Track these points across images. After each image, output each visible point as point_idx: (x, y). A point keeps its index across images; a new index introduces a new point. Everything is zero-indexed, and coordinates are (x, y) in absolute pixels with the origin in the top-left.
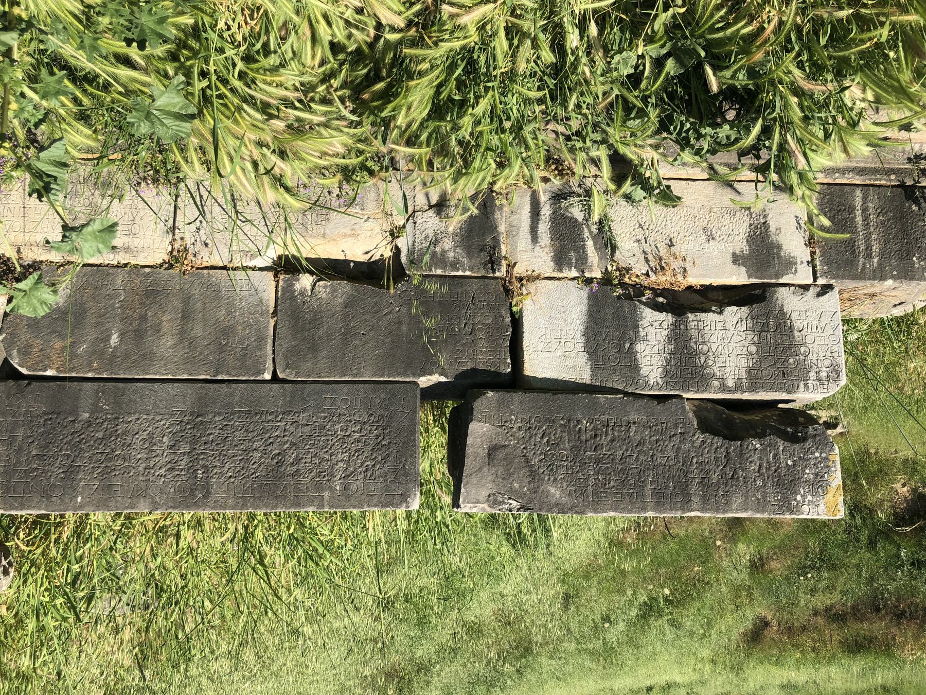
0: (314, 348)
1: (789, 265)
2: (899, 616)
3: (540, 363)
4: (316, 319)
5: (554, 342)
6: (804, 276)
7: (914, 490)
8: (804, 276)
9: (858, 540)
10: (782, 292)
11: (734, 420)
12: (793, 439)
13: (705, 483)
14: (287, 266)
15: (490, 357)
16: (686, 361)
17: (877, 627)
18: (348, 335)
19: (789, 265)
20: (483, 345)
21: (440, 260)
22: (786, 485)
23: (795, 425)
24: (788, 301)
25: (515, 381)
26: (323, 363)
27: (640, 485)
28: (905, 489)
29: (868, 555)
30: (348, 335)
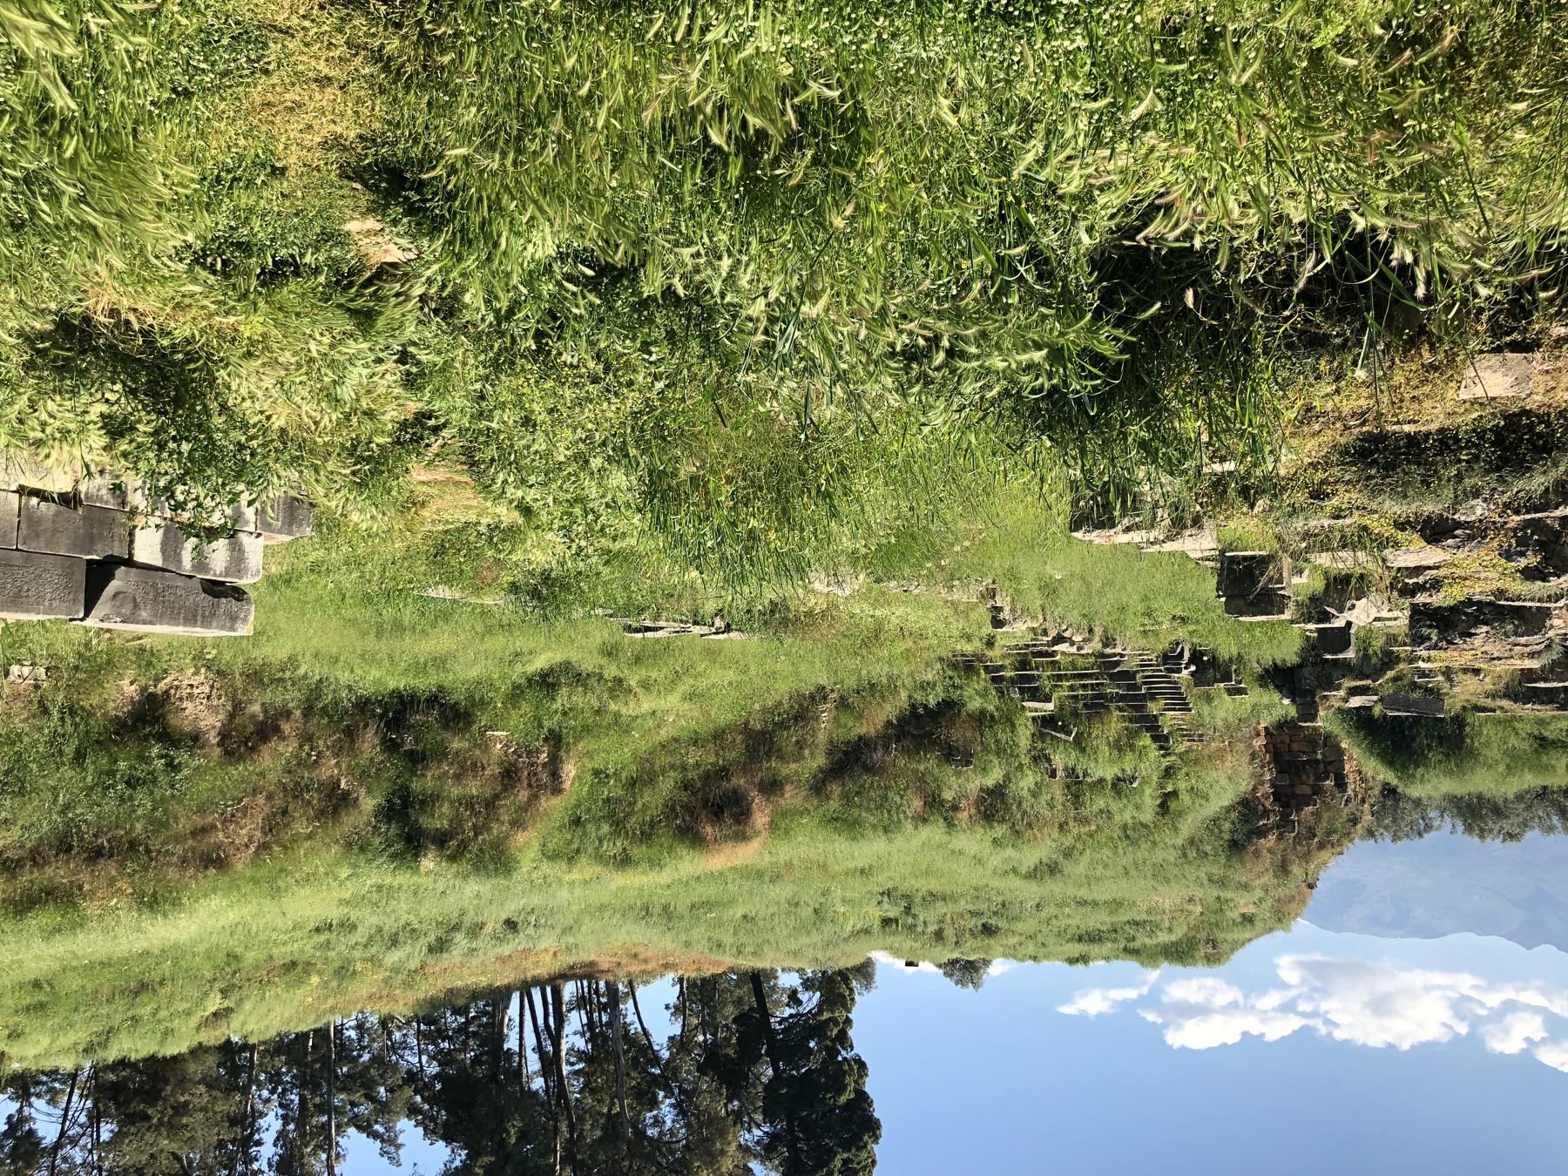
0: (38, 536)
1: (247, 522)
2: (95, 855)
3: (141, 556)
4: (39, 521)
5: (148, 548)
6: (251, 528)
7: (144, 689)
8: (251, 528)
9: (61, 753)
10: (241, 535)
11: (215, 589)
12: (238, 600)
13: (203, 616)
14: (21, 491)
15: (118, 550)
16: (201, 562)
17: (57, 873)
18: (55, 531)
19: (247, 522)
20: (116, 544)
21: (100, 499)
22: (233, 619)
23: (238, 594)
24: (242, 537)
25: (130, 562)
26: (42, 544)
27: (195, 616)
28: (133, 687)
29: (71, 773)
30: (55, 531)
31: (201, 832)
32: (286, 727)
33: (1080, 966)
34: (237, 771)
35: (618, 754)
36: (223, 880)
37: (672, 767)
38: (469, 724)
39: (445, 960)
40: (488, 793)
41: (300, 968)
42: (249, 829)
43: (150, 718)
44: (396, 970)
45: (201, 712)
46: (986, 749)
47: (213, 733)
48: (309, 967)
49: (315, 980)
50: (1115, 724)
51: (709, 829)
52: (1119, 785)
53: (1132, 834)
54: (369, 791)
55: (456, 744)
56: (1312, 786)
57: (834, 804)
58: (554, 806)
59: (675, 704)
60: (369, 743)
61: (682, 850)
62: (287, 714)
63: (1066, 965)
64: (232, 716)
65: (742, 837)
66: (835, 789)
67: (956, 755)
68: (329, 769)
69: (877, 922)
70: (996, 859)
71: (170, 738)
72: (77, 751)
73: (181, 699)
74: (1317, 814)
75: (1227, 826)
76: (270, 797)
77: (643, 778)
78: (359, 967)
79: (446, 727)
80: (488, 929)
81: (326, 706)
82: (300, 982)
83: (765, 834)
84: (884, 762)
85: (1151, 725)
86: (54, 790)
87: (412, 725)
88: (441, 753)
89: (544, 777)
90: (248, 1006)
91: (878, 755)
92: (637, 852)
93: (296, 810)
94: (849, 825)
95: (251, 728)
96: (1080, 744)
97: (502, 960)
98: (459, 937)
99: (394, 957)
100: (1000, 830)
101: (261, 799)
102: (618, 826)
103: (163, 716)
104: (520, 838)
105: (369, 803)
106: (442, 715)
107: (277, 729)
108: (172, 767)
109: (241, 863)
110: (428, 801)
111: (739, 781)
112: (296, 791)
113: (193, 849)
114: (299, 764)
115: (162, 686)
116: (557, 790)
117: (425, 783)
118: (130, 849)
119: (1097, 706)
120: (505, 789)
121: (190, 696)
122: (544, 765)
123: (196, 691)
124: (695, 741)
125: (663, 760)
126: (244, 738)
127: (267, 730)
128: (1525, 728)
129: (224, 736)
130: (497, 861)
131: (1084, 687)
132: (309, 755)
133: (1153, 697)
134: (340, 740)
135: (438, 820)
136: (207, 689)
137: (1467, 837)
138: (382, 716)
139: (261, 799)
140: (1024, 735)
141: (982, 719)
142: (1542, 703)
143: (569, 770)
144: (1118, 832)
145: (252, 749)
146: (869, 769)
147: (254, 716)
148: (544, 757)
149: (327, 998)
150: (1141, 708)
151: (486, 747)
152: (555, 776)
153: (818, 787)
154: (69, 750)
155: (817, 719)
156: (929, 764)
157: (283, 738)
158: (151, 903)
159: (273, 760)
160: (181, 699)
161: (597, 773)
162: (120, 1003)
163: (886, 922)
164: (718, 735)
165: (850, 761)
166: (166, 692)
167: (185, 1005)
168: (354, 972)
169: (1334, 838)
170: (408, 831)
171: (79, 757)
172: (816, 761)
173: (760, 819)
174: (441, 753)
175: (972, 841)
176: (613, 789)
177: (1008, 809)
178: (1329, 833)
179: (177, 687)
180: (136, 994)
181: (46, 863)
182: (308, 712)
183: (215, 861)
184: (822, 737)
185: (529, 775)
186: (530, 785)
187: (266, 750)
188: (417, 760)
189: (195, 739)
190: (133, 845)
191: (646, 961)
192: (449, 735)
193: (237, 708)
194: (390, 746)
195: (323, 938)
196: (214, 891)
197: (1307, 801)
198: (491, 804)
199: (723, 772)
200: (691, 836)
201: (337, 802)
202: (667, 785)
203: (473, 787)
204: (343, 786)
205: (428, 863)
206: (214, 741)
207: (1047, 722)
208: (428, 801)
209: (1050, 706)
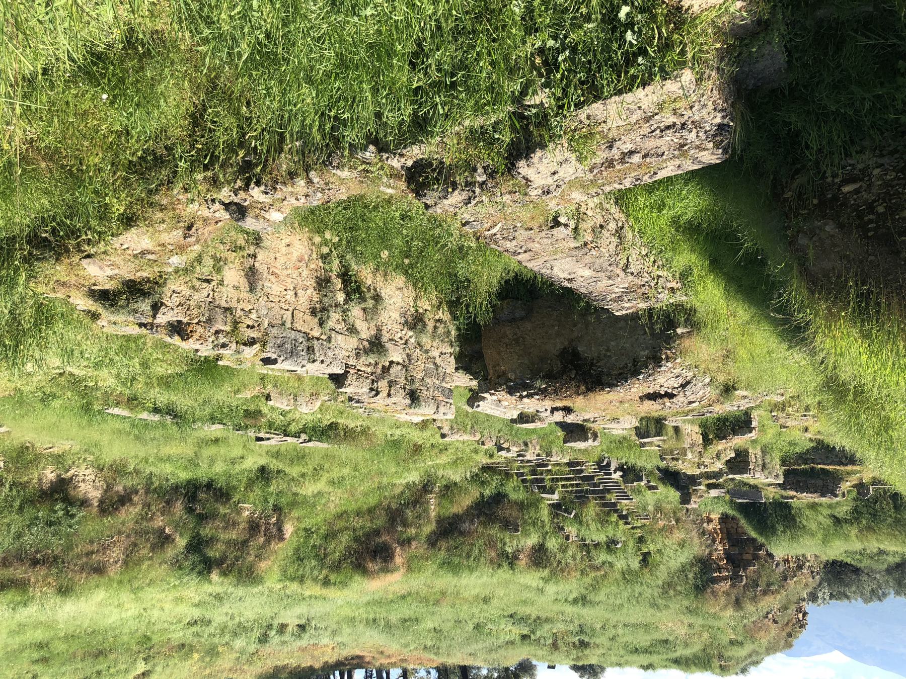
2: (35, 563)
7: (58, 476)
9: (12, 506)
17: (19, 572)
31: (89, 554)
32: (136, 499)
33: (650, 671)
34: (108, 521)
35: (316, 519)
36: (104, 580)
37: (347, 529)
38: (228, 499)
39: (267, 649)
40: (243, 537)
41: (186, 649)
42: (116, 553)
43: (61, 491)
44: (242, 652)
45: (89, 487)
46: (525, 522)
47: (96, 500)
48: (192, 649)
49: (196, 656)
50: (592, 510)
51: (370, 565)
52: (611, 545)
53: (628, 577)
54: (181, 535)
55: (223, 510)
56: (753, 555)
57: (442, 554)
58: (282, 549)
59: (334, 488)
60: (179, 508)
61: (357, 578)
62: (136, 492)
63: (642, 671)
64: (106, 491)
65: (386, 570)
66: (443, 544)
67: (510, 525)
68: (159, 522)
69: (518, 638)
70: (551, 589)
71: (69, 501)
72: (21, 505)
73: (78, 482)
74: (758, 572)
75: (691, 575)
76: (128, 536)
77: (331, 535)
78: (220, 649)
79: (216, 501)
80: (290, 629)
81: (156, 488)
82: (187, 656)
83: (402, 570)
84: (470, 529)
85: (612, 507)
86: (9, 525)
87: (200, 497)
88: (214, 515)
89: (274, 531)
90: (159, 669)
91: (466, 526)
92: (332, 577)
93: (141, 542)
94: (449, 566)
95: (116, 499)
96: (578, 520)
97: (303, 650)
98: (272, 633)
99: (239, 643)
100: (546, 573)
101: (123, 537)
102: (321, 560)
103: (67, 489)
104: (263, 565)
105: (181, 542)
106: (215, 494)
107: (130, 500)
108: (67, 514)
109: (113, 571)
110: (211, 541)
111: (385, 538)
112: (141, 533)
113: (86, 563)
114: (142, 519)
115: (70, 474)
116: (281, 539)
117: (206, 531)
118: (52, 561)
119: (582, 498)
120: (251, 536)
121: (84, 480)
122: (274, 524)
123: (87, 478)
124: (358, 513)
125: (340, 524)
126: (112, 503)
127: (125, 499)
128: (826, 512)
129: (101, 502)
130: (248, 576)
131: (572, 485)
132: (147, 514)
133: (609, 491)
134: (163, 507)
135: (213, 553)
136: (93, 477)
137: (898, 597)
138: (186, 495)
139: (123, 537)
140: (545, 513)
141: (521, 506)
142: (811, 493)
143: (289, 529)
144: (619, 576)
145: (116, 509)
146: (462, 534)
147: (118, 491)
148: (274, 520)
149: (205, 668)
150: (603, 498)
151: (239, 512)
152: (280, 530)
153: (433, 542)
154: (17, 504)
155: (428, 503)
156: (494, 530)
157: (133, 504)
158: (64, 591)
159: (129, 514)
160: (78, 482)
161: (306, 530)
162: (89, 660)
163: (524, 637)
164: (370, 511)
165: (449, 529)
166: (71, 478)
167: (124, 666)
168: (218, 653)
169: (773, 588)
170: (202, 559)
171: (21, 509)
172: (429, 528)
173: (398, 560)
174: (214, 515)
175: (532, 578)
176: (315, 540)
177: (548, 560)
178: (769, 585)
179: (77, 476)
180: (97, 656)
181: (11, 565)
182: (147, 492)
183: (99, 570)
184: (433, 514)
185: (262, 530)
186: (265, 535)
187: (123, 510)
188: (202, 518)
189: (84, 503)
190: (55, 558)
191: (389, 657)
192: (218, 505)
193: (109, 487)
194: (190, 511)
195: (195, 629)
196: (97, 586)
197: (748, 564)
198: (245, 543)
199: (377, 532)
200: (360, 568)
201: (163, 540)
202: (345, 539)
203: (233, 535)
204: (167, 531)
205: (215, 576)
206: (96, 504)
207: (556, 507)
208: (211, 541)
209: (556, 497)
